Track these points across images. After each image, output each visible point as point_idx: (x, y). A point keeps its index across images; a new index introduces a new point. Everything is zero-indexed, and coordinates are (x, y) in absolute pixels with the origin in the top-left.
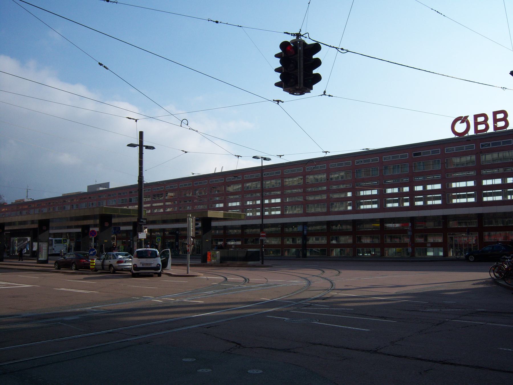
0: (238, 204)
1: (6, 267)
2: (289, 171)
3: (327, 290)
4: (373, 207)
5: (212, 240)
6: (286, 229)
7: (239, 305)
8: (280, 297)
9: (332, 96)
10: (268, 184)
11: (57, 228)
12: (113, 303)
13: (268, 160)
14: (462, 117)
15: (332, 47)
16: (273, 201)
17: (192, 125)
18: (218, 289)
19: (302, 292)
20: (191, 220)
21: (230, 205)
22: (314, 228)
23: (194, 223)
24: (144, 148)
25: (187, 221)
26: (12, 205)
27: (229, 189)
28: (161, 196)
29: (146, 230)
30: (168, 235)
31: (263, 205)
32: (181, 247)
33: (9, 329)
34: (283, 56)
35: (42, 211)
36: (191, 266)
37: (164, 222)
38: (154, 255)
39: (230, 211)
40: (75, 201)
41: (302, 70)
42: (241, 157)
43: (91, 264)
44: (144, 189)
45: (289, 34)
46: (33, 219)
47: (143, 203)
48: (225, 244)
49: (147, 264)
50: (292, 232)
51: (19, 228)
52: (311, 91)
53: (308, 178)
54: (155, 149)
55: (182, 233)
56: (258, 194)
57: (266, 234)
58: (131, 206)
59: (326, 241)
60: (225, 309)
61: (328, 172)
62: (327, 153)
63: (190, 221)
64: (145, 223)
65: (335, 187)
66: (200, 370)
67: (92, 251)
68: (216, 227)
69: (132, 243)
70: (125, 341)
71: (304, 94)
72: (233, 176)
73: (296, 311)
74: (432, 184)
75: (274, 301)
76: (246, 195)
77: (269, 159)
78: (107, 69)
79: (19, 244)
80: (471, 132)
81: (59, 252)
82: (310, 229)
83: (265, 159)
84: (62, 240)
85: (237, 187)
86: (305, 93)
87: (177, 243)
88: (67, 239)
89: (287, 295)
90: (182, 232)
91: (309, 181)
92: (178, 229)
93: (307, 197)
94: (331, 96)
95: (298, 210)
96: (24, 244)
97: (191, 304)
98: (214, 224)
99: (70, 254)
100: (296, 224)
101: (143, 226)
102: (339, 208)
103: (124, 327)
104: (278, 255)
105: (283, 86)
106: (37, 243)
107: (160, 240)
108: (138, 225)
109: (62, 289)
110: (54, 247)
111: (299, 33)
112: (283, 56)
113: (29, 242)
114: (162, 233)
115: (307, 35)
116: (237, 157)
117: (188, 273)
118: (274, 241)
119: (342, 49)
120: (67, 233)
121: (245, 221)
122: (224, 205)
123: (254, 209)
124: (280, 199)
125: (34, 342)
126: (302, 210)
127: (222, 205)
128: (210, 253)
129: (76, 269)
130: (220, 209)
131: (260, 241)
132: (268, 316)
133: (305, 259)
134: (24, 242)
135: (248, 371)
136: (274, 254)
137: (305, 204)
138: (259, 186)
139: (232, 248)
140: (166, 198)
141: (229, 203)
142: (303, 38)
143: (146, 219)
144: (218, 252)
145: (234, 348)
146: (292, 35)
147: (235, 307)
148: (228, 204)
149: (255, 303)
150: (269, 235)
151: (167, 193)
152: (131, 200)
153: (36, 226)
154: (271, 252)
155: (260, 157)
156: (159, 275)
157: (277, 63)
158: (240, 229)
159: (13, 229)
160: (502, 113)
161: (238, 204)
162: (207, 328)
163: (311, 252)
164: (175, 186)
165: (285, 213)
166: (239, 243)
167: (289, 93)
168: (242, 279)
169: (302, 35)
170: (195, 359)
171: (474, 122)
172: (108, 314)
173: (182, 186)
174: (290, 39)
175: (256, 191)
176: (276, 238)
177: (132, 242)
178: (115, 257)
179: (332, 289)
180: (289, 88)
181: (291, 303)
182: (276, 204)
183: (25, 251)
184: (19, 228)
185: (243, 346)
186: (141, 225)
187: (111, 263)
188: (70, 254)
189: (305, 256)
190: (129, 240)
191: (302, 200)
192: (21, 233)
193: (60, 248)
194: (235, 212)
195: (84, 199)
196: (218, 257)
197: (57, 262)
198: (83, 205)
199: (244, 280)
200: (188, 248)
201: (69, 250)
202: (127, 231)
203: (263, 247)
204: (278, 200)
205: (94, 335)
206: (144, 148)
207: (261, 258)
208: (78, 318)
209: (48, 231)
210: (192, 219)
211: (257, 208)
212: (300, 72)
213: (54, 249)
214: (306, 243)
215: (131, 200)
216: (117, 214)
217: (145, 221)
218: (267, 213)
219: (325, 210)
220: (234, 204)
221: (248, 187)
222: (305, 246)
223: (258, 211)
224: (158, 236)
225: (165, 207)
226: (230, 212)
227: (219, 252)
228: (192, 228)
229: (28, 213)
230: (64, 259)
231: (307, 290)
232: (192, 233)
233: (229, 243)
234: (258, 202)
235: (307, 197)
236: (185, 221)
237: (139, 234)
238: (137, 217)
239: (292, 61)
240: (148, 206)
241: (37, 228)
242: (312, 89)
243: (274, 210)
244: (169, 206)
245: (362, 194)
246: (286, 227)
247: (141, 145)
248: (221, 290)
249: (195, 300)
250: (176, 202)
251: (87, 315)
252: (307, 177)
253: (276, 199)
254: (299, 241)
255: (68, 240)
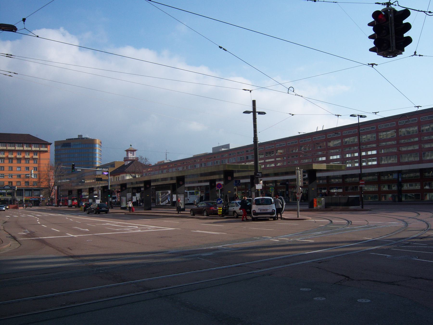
0: (338, 157)
1: (154, 214)
2: (383, 126)
3: (423, 230)
5: (317, 188)
6: (382, 177)
7: (346, 244)
8: (380, 237)
9: (423, 56)
10: (364, 138)
11: (190, 183)
12: (238, 242)
13: (364, 117)
15: (420, 11)
16: (369, 153)
17: (296, 91)
18: (325, 230)
19: (400, 232)
20: (300, 172)
21: (331, 158)
22: (407, 175)
23: (302, 175)
24: (257, 114)
25: (295, 173)
26: (156, 165)
27: (330, 144)
28: (272, 153)
29: (262, 182)
30: (279, 186)
31: (360, 157)
32: (291, 196)
33: (161, 262)
34: (376, 24)
35: (178, 170)
36: (301, 211)
37: (276, 175)
38: (269, 202)
39: (332, 163)
40: (203, 160)
41: (394, 35)
42: (341, 116)
43: (219, 211)
44: (258, 147)
45: (380, 4)
46: (172, 176)
47: (258, 160)
48: (329, 192)
49: (264, 210)
50: (388, 179)
51: (162, 184)
52: (403, 53)
53: (401, 131)
54: (266, 114)
55: (291, 183)
57: (365, 182)
58: (248, 163)
59: (420, 187)
60: (333, 247)
61: (420, 124)
62: (419, 107)
63: (298, 174)
64: (260, 176)
65: (426, 138)
66: (316, 298)
67: (219, 201)
68: (320, 177)
69: (250, 193)
70: (251, 273)
71: (397, 56)
72: (334, 133)
73: (396, 249)
75: (375, 240)
76: (346, 149)
77: (365, 117)
78: (226, 50)
79: (162, 196)
81: (193, 201)
82: (404, 176)
83: (361, 116)
84: (194, 192)
85: (337, 142)
86: (398, 55)
87: (287, 192)
88: (198, 191)
89: (387, 235)
90: (291, 182)
91: (401, 134)
92: (287, 180)
93: (400, 148)
94: (421, 56)
95: (393, 160)
96: (166, 196)
97: (303, 243)
98: (318, 175)
99: (202, 203)
100: (392, 173)
101: (259, 179)
102: (431, 157)
103: (249, 262)
104: (377, 200)
105: (377, 51)
106: (176, 195)
107: (273, 190)
108: (255, 178)
109: (198, 231)
110: (188, 198)
111: (389, 2)
112: (376, 24)
113: (169, 194)
114: (274, 184)
115: (396, 3)
116: (337, 116)
117: (298, 217)
118: (372, 188)
119: (430, 12)
120: (198, 186)
121: (345, 171)
122: (326, 158)
123: (353, 161)
124: (375, 151)
125: (180, 273)
126: (397, 160)
127: (324, 159)
128: (316, 200)
129: (207, 215)
130: (323, 162)
131: (359, 189)
132: (371, 253)
133: (401, 203)
134: (166, 194)
135: (357, 300)
136: (372, 199)
137: (399, 154)
138: (356, 140)
139: (335, 195)
140: (277, 154)
141: (331, 157)
142: (393, 6)
143: (261, 173)
144: (323, 199)
145: (344, 280)
146: (382, 5)
147: (341, 246)
148: (329, 158)
149: (358, 242)
150: (368, 183)
151: (277, 151)
152: (247, 158)
153: (174, 181)
154: (370, 198)
155: (357, 115)
156: (274, 219)
157: (371, 31)
158: (341, 179)
159: (157, 184)
161: (338, 157)
162: (319, 263)
163: (406, 196)
164: (283, 144)
165: (381, 163)
166: (341, 190)
167: (382, 57)
168: (345, 221)
169: (391, 3)
170: (311, 289)
171: (253, 123)
172: (235, 251)
173: (289, 143)
174: (380, 8)
175: (354, 145)
176: (373, 185)
177: (250, 192)
178: (238, 205)
179: (428, 229)
180: (382, 52)
181: (391, 242)
182: (372, 156)
183: (167, 201)
184: (162, 184)
185: (351, 278)
186: (258, 178)
187: (235, 210)
188: (202, 203)
189: (400, 200)
190: (248, 190)
191: (396, 151)
192: (163, 188)
193: (194, 199)
194: (336, 164)
195: (210, 158)
196: (323, 203)
197: (191, 210)
198: (210, 164)
199: (347, 223)
200: (297, 196)
201: (201, 199)
202: (245, 184)
203: (362, 194)
204: (374, 152)
205: (226, 268)
206: (257, 114)
207: (361, 203)
208: (213, 254)
209: (184, 185)
210: (300, 171)
211: (363, 159)
212: (392, 37)
213: (188, 200)
214: (401, 189)
215: (248, 157)
216: (238, 169)
217: (260, 175)
218: (364, 164)
219: (417, 159)
220: (335, 157)
221: (346, 142)
222: (400, 192)
223: (356, 162)
224: (271, 186)
225: (275, 162)
226: (331, 164)
227: (323, 198)
228: (300, 179)
229: (168, 172)
230: (198, 207)
231: (405, 230)
232: (300, 184)
233: (332, 191)
234: (356, 155)
235: (400, 148)
236: (294, 173)
237: (256, 186)
238: (254, 172)
239: (384, 28)
240: (262, 162)
241: (175, 183)
242: (404, 51)
243: (370, 161)
244: (279, 161)
245: (321, 160)
246: (382, 176)
247: (254, 112)
248: (328, 231)
249: (306, 239)
250: (285, 158)
251: (219, 251)
252: (400, 130)
253: (372, 151)
254: (395, 188)
255: (199, 192)
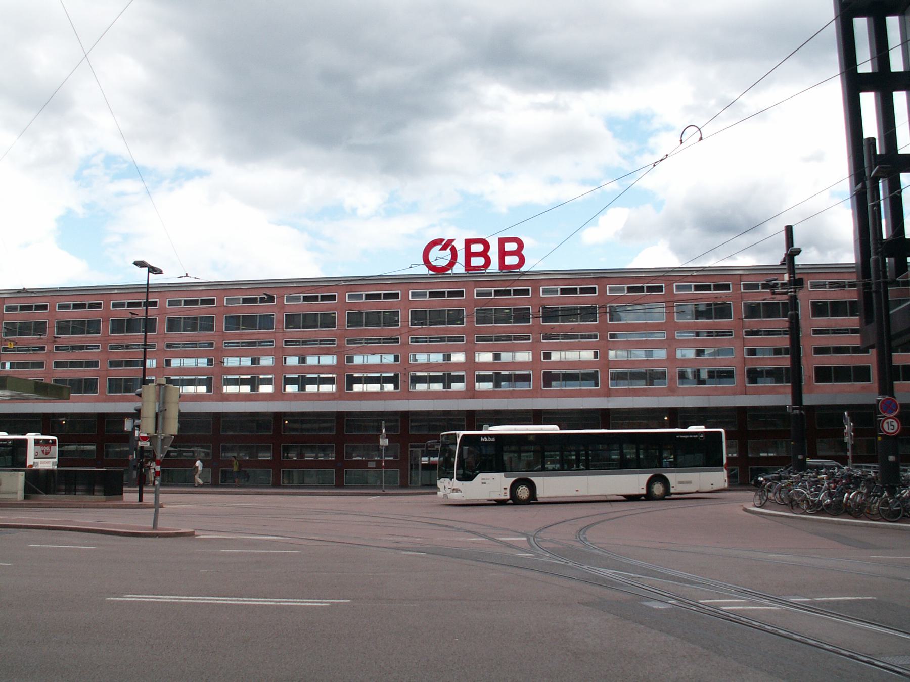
4: (241, 391)
14: (443, 240)
56: (661, 336)
74: (561, 350)
80: (459, 268)
160: (516, 243)
